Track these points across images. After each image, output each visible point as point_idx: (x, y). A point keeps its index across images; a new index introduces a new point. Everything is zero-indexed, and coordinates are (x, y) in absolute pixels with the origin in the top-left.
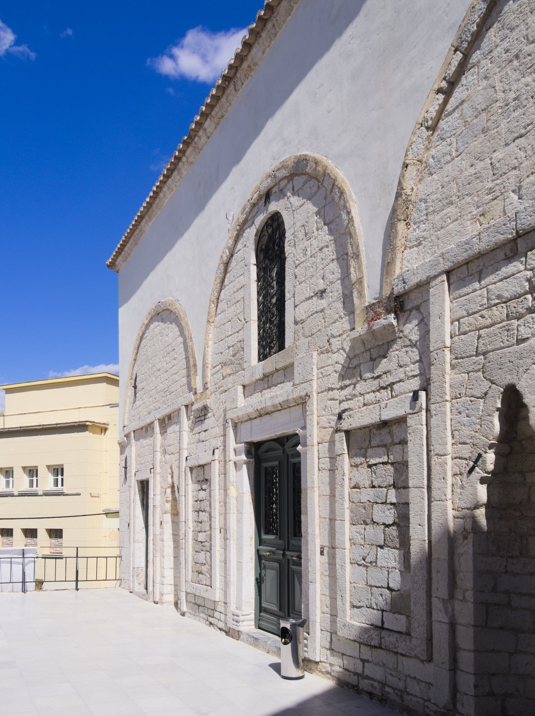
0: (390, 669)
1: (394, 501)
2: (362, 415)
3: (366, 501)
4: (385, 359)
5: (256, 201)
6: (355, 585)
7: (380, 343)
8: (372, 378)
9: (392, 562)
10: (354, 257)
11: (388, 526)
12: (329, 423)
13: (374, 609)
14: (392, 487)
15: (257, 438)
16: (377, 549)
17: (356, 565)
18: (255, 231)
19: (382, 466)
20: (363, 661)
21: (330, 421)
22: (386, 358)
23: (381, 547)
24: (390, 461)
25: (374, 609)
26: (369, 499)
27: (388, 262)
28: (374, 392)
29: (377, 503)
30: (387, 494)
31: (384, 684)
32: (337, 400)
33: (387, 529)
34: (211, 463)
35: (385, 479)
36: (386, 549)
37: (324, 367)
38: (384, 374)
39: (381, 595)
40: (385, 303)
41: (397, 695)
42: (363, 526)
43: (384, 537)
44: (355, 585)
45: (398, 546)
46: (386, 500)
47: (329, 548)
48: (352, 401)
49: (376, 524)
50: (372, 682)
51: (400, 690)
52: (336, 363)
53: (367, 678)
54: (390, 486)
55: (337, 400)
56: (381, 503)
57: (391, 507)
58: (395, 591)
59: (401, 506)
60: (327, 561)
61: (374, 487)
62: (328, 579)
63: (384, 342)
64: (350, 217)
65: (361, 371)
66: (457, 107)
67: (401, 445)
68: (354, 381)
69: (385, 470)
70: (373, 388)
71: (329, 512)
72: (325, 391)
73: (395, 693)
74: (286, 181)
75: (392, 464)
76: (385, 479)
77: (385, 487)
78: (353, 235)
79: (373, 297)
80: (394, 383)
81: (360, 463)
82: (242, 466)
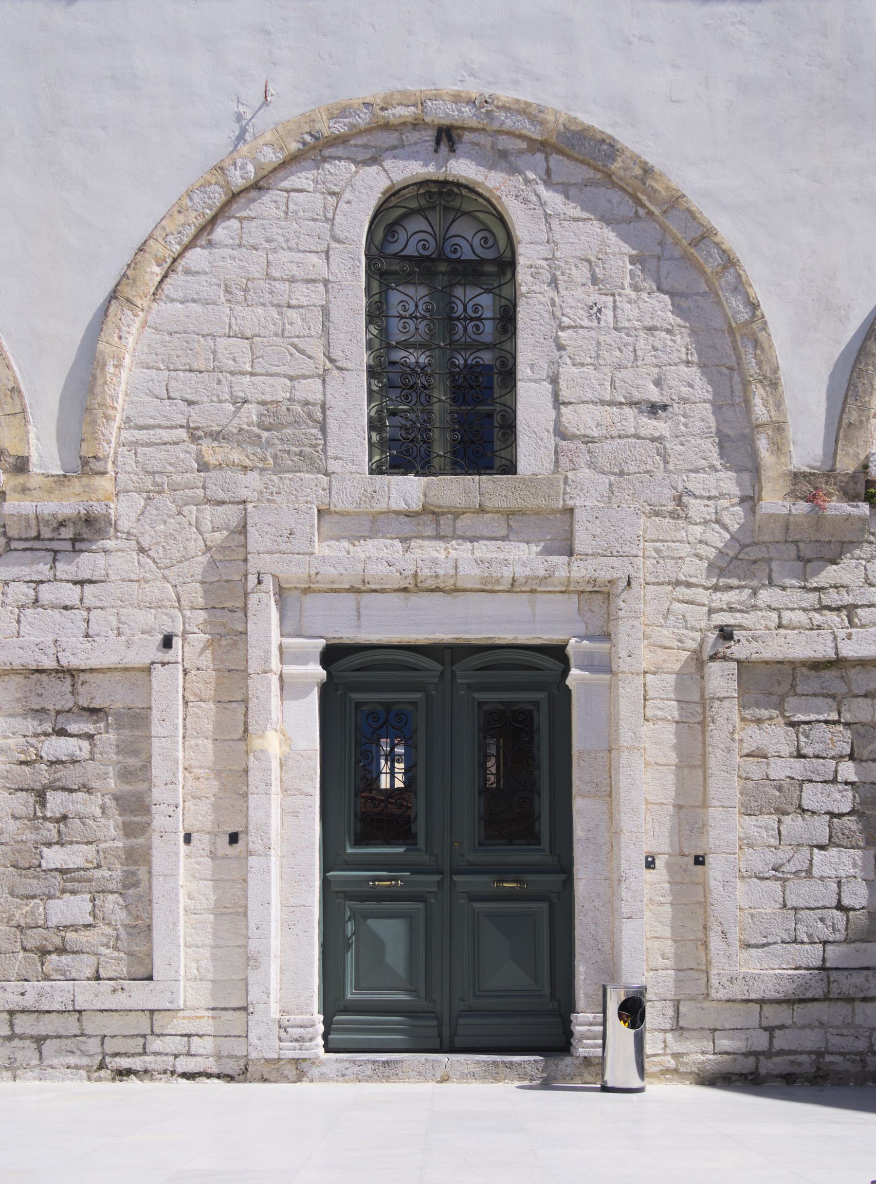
0: (837, 1027)
1: (853, 778)
2: (788, 640)
3: (783, 778)
4: (834, 567)
5: (396, 122)
6: (752, 911)
7: (824, 539)
8: (804, 588)
9: (847, 868)
10: (765, 383)
11: (840, 816)
12: (680, 641)
13: (802, 943)
14: (847, 759)
15: (349, 635)
16: (811, 851)
17: (755, 880)
18: (383, 184)
19: (825, 726)
20: (770, 1030)
21: (683, 638)
22: (836, 564)
23: (822, 847)
24: (842, 720)
25: (802, 943)
26: (790, 774)
27: (850, 424)
28: (804, 610)
29: (810, 781)
30: (836, 767)
31: (820, 1054)
32: (704, 605)
33: (835, 820)
34: (148, 670)
35: (830, 746)
36: (833, 851)
37: (667, 541)
38: (831, 587)
39: (822, 920)
40: (841, 482)
41: (853, 1061)
42: (775, 817)
43: (830, 832)
44: (752, 911)
45: (862, 844)
46: (836, 777)
47: (670, 855)
48: (746, 615)
49: (809, 813)
50: (790, 1057)
51: (860, 1053)
52: (701, 542)
53: (781, 1052)
54: (842, 757)
55: (704, 605)
56: (821, 782)
57: (846, 787)
58: (854, 909)
59: (867, 787)
60: (666, 878)
61: (800, 756)
62: (670, 910)
63: (833, 540)
64: (758, 313)
65: (771, 570)
66: (589, 165)
67: (869, 699)
68: (754, 583)
69: (832, 733)
70: (804, 605)
71: (674, 794)
72: (669, 583)
73: (849, 1060)
74: (524, 145)
75: (847, 725)
76: (830, 746)
77: (832, 758)
78: (766, 346)
79: (806, 463)
80: (857, 606)
81: (768, 717)
82: (313, 689)
